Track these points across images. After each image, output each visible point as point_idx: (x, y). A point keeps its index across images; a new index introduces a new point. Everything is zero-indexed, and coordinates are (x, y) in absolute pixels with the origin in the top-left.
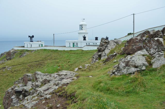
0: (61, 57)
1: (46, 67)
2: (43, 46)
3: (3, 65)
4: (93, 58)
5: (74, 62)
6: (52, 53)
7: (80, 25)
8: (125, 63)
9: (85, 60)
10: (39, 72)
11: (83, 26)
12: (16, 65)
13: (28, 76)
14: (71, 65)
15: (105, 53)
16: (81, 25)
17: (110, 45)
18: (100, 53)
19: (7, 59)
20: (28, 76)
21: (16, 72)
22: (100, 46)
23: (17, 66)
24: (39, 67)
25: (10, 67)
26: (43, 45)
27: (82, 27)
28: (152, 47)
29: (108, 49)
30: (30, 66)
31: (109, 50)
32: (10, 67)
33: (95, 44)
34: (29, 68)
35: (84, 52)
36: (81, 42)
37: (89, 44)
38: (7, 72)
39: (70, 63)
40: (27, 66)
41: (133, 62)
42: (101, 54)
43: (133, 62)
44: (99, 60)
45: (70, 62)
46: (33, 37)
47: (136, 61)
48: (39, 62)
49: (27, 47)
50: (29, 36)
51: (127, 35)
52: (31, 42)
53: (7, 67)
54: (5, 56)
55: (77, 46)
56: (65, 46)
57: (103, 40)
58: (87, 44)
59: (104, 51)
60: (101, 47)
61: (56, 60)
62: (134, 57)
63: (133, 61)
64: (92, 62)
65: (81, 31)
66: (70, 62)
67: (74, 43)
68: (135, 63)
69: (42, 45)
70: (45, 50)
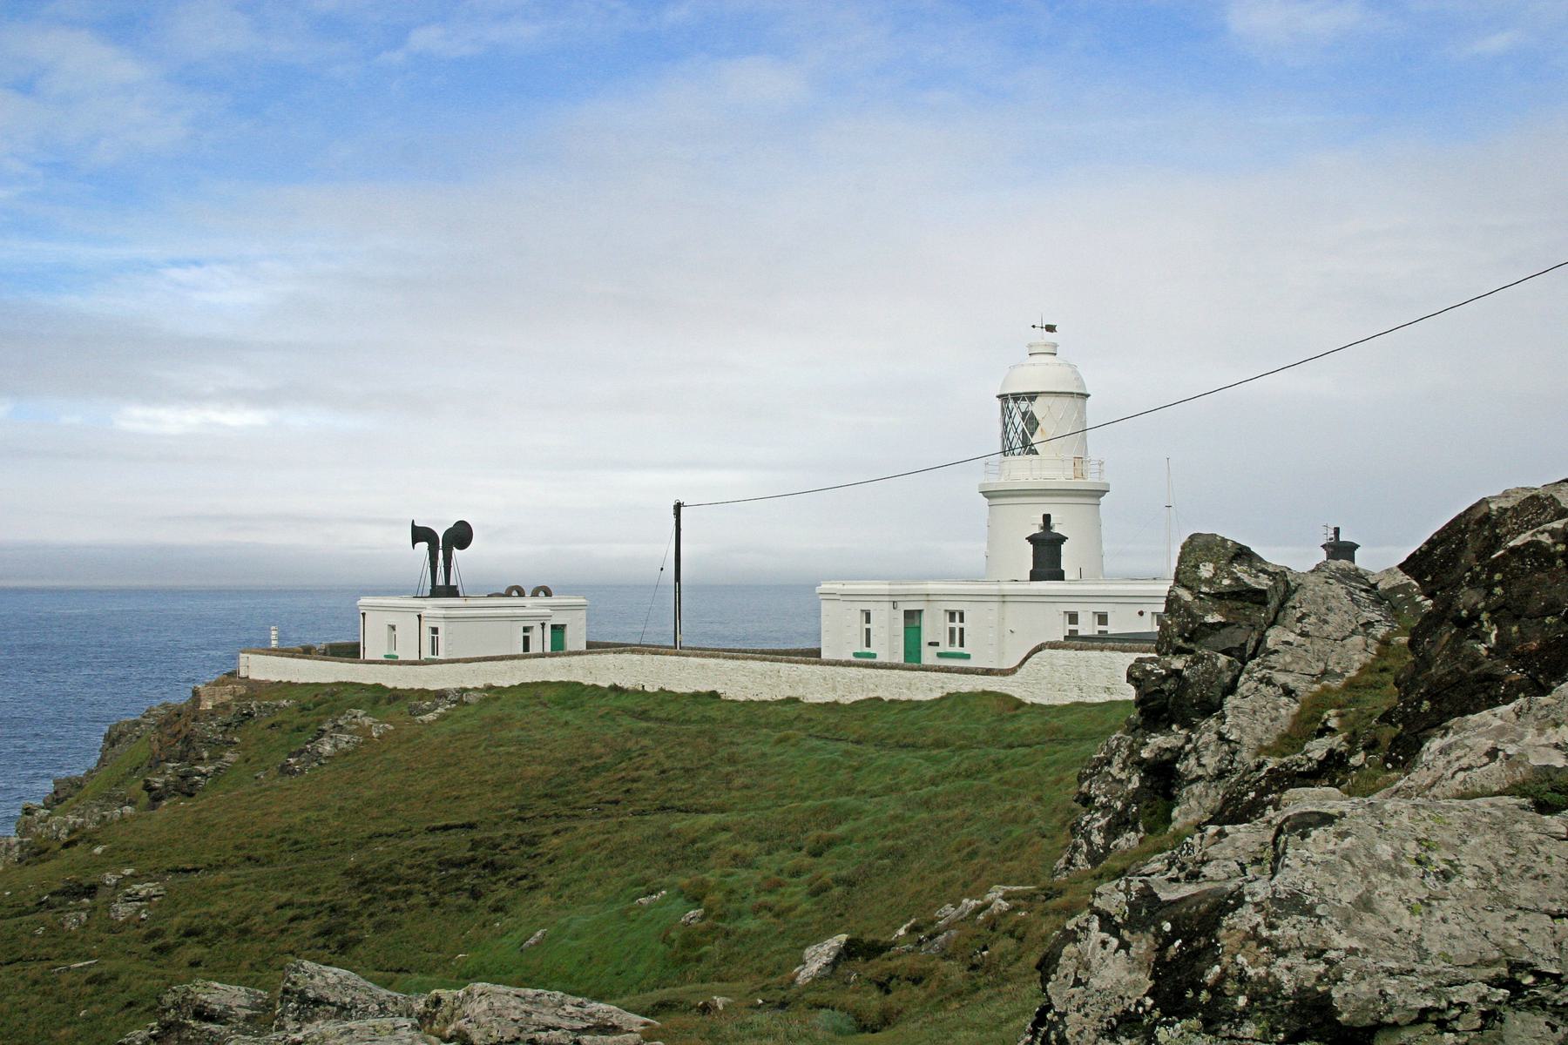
0: (738, 782)
1: (542, 899)
2: (571, 645)
3: (78, 852)
4: (1086, 800)
5: (889, 853)
6: (646, 732)
7: (1003, 398)
8: (1143, 945)
9: (1018, 831)
10: (333, 974)
11: (1038, 408)
12: (210, 867)
13: (211, 1018)
14: (837, 891)
15: (1221, 737)
16: (1016, 397)
17: (1310, 624)
18: (1158, 741)
19: (148, 788)
20: (202, 1014)
21: (197, 951)
22: (1163, 643)
23: (222, 876)
24: (464, 899)
25: (143, 889)
26: (569, 632)
27: (1031, 421)
28: (1446, 617)
29: (1269, 682)
30: (362, 880)
31: (1288, 692)
32: (143, 889)
33: (1087, 627)
34: (354, 903)
35: (1025, 724)
36: (1003, 598)
37: (1103, 619)
38: (108, 937)
39: (827, 869)
40: (332, 877)
41: (1287, 930)
42: (1178, 754)
43: (1287, 930)
44: (1150, 830)
45: (830, 843)
46: (461, 535)
47: (1365, 904)
48: (477, 835)
49: (391, 660)
50: (420, 534)
51: (1039, 399)
52: (436, 592)
53: (110, 878)
54: (142, 752)
55: (956, 649)
56: (817, 653)
57: (1206, 571)
58: (1073, 618)
59: (1211, 708)
60: (1179, 651)
61: (679, 823)
62: (1326, 819)
63: (1294, 903)
64: (1061, 863)
65: (1021, 471)
66: (830, 843)
67: (912, 617)
68: (1317, 954)
69: (558, 630)
70: (573, 694)
